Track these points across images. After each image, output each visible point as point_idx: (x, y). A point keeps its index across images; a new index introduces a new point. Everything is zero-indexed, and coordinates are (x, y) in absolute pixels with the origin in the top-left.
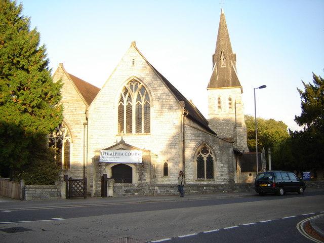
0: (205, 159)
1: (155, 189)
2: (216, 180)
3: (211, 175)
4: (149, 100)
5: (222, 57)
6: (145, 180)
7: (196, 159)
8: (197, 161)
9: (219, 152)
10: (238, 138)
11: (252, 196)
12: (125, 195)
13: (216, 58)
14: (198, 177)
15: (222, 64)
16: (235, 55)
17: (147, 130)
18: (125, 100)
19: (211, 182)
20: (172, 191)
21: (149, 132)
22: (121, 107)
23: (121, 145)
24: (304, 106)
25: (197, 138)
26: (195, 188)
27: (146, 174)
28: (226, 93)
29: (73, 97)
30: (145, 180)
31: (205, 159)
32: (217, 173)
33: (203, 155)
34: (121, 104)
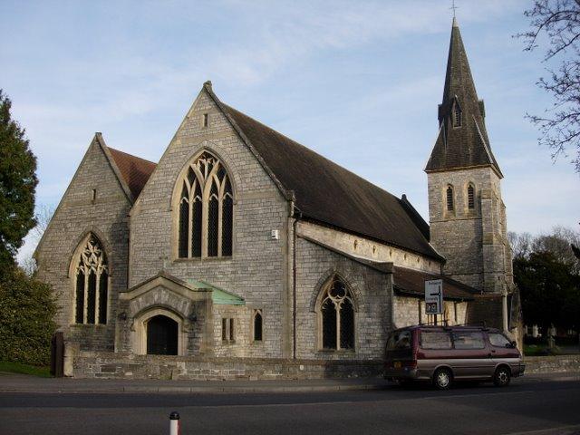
0: (338, 308)
1: (175, 366)
2: (358, 351)
3: (349, 340)
4: (231, 193)
5: (454, 109)
6: (198, 348)
7: (318, 308)
8: (323, 311)
9: (363, 293)
10: (485, 267)
11: (374, 390)
12: (102, 375)
13: (444, 113)
14: (324, 346)
15: (455, 122)
16: (481, 104)
17: (228, 251)
18: (192, 192)
19: (348, 356)
20: (217, 371)
21: (231, 254)
22: (185, 207)
23: (160, 278)
24: (34, 192)
25: (321, 265)
26: (277, 367)
27: (200, 335)
28: (462, 179)
29: (114, 193)
30: (198, 348)
31: (338, 308)
32: (359, 339)
33: (334, 300)
34: (214, 197)
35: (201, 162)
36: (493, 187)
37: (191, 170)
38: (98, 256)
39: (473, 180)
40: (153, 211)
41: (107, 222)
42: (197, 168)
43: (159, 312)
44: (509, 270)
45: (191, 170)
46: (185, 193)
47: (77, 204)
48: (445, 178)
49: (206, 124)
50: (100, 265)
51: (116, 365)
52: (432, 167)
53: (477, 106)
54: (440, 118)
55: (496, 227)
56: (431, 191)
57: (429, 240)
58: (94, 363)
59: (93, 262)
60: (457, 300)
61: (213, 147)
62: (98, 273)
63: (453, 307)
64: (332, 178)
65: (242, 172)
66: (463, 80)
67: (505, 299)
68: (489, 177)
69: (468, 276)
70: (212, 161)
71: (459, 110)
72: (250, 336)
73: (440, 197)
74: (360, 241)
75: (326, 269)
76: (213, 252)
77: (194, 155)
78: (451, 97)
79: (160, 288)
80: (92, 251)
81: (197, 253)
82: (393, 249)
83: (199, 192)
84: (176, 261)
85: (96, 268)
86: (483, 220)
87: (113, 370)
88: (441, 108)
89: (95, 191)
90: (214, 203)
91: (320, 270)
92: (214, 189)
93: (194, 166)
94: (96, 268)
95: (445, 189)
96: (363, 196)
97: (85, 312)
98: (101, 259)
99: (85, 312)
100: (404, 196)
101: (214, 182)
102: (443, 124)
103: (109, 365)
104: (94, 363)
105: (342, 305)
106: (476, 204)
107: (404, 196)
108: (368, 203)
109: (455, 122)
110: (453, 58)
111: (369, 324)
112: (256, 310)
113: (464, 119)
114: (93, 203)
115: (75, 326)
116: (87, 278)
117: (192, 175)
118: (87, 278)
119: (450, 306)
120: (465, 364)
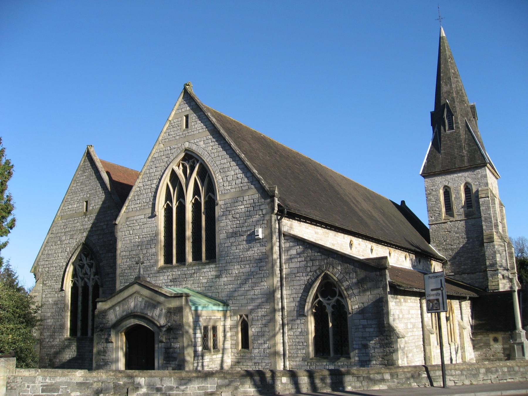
0: (329, 310)
15: (447, 128)
16: (473, 108)
17: (212, 257)
22: (168, 211)
31: (329, 310)
35: (183, 165)
36: (490, 186)
37: (173, 173)
38: (91, 266)
39: (469, 180)
40: (138, 218)
41: (99, 232)
42: (180, 172)
43: (133, 322)
44: (513, 268)
45: (173, 173)
46: (168, 197)
47: (72, 216)
48: (441, 181)
49: (187, 126)
50: (92, 277)
51: (61, 383)
52: (427, 174)
53: (469, 109)
54: (433, 124)
55: (496, 226)
56: (428, 195)
57: (429, 243)
58: (34, 382)
59: (86, 274)
60: (461, 299)
61: (194, 148)
62: (91, 284)
63: (458, 306)
64: (326, 180)
65: (223, 171)
66: (454, 86)
67: (516, 295)
68: (485, 176)
69: (472, 276)
70: (194, 163)
71: (450, 115)
72: (237, 344)
73: (438, 200)
74: (356, 241)
75: (314, 268)
76: (197, 256)
77: (176, 157)
78: (442, 102)
79: (135, 295)
80: (85, 263)
81: (181, 259)
82: (392, 250)
83: (181, 196)
84: (162, 268)
85: (89, 279)
86: (483, 219)
87: (57, 390)
88: (433, 115)
89: (87, 202)
90: (196, 205)
91: (309, 269)
92: (196, 192)
93: (176, 168)
94: (89, 279)
95: (441, 192)
96: (360, 199)
97: (79, 324)
98: (93, 270)
99: (79, 324)
100: (403, 202)
101: (195, 179)
102: (436, 129)
103: (52, 385)
104: (34, 382)
105: (333, 307)
106: (474, 203)
107: (403, 202)
108: (366, 206)
109: (447, 128)
110: (442, 66)
111: (364, 327)
112: (241, 316)
113: (457, 123)
114: (85, 214)
115: (69, 339)
116: (80, 290)
117: (174, 177)
118: (80, 290)
119: (455, 303)
120: (198, 179)
